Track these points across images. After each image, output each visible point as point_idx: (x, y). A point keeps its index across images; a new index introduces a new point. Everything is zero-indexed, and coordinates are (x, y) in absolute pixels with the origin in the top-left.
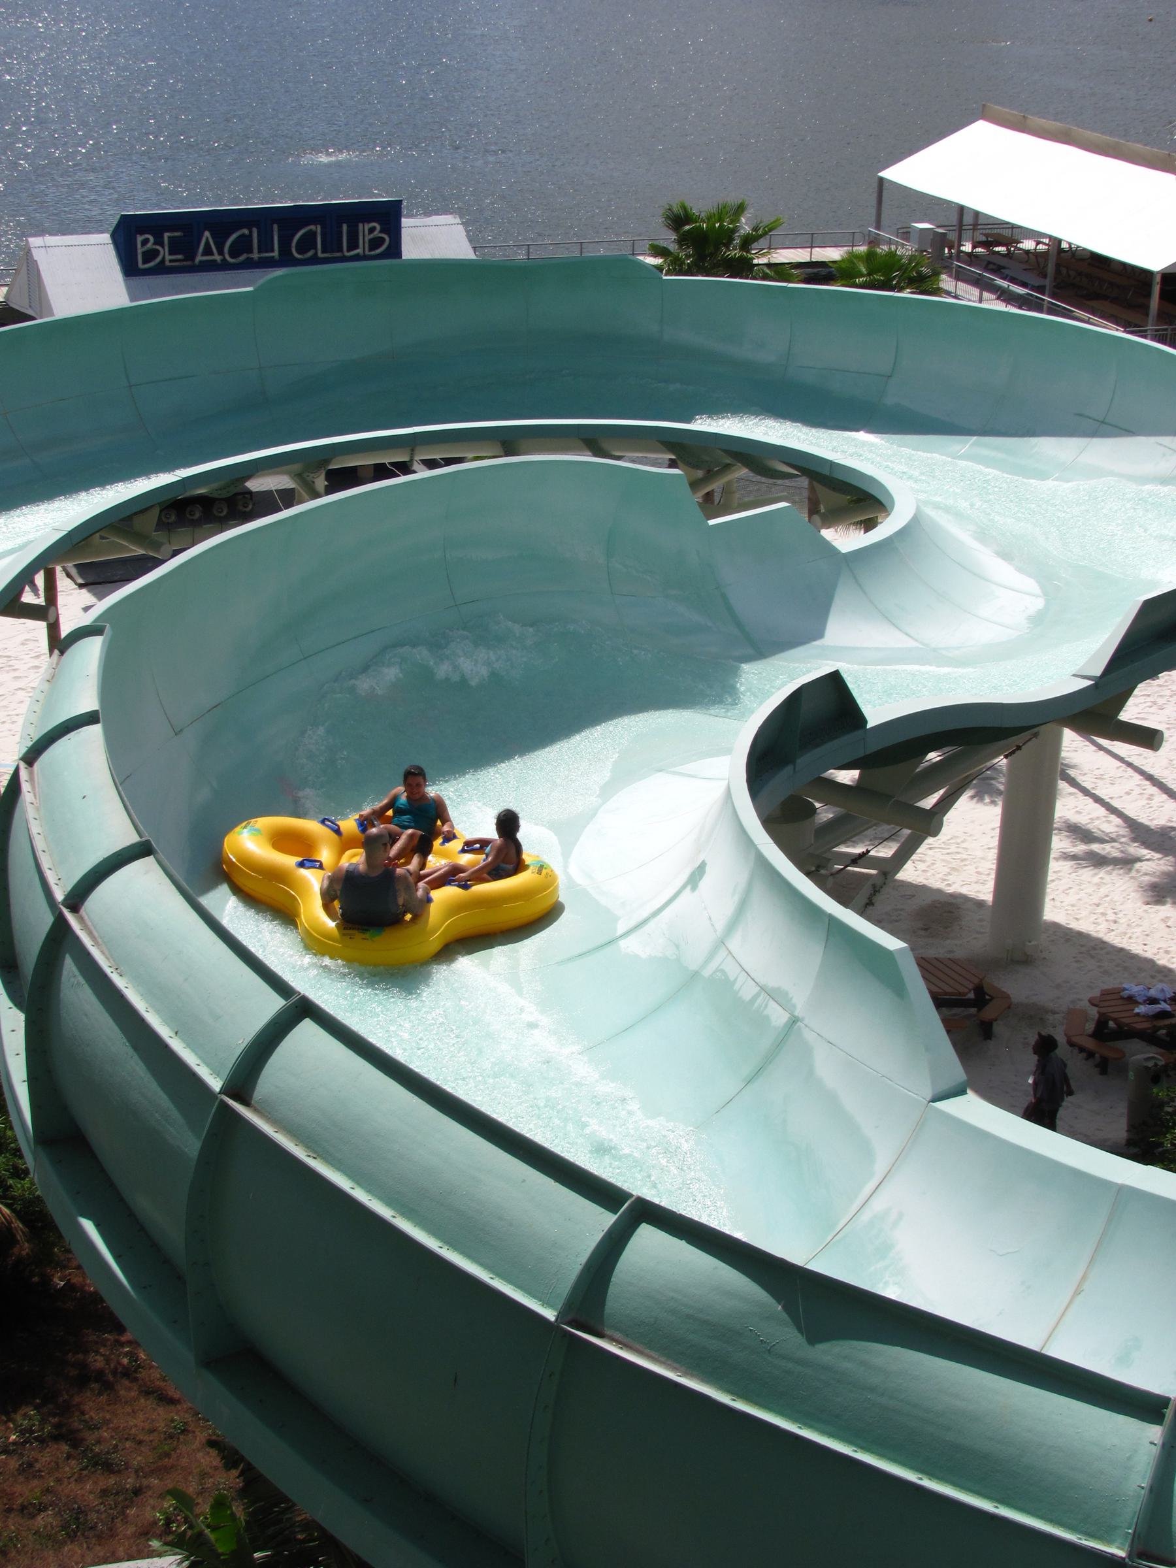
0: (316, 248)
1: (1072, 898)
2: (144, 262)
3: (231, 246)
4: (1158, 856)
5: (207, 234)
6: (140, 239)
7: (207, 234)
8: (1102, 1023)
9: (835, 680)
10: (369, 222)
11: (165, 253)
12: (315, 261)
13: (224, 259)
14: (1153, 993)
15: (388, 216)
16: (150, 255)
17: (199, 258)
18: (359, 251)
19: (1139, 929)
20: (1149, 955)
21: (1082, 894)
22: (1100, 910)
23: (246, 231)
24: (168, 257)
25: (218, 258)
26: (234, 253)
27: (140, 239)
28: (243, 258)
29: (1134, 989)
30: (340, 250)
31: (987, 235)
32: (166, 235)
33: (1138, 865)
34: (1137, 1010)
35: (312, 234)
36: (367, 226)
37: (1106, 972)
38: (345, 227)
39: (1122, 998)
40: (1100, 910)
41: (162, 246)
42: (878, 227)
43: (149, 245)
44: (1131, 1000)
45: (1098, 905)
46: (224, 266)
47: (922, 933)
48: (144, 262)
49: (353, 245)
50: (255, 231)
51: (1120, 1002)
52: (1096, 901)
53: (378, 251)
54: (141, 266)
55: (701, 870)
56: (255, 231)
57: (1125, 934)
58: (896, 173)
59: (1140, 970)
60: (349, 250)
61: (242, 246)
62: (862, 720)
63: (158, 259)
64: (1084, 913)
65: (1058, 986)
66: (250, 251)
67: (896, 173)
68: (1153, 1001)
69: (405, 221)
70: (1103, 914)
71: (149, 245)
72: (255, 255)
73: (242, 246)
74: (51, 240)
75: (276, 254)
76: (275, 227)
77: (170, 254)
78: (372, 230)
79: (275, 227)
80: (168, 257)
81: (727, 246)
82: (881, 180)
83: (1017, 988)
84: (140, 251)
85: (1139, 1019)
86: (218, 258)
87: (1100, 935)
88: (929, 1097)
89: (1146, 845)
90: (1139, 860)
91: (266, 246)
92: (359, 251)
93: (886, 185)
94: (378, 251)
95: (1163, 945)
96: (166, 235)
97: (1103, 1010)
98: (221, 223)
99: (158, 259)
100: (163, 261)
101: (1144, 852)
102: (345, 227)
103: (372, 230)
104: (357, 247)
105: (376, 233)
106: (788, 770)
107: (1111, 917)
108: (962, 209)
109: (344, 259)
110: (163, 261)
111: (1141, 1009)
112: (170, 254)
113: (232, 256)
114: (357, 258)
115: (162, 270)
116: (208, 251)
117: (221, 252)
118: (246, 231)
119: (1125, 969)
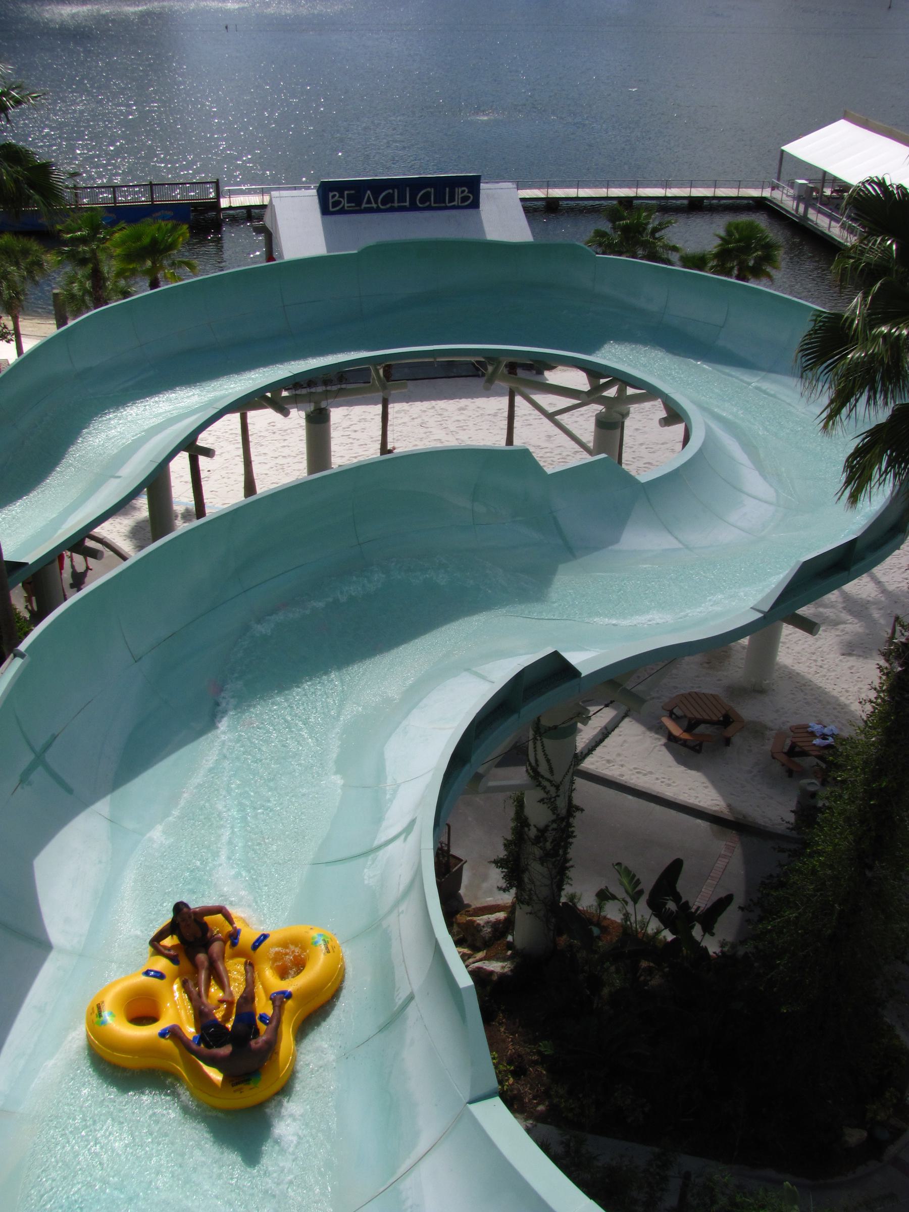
0: (430, 201)
1: (798, 648)
2: (333, 207)
3: (384, 197)
4: (856, 621)
5: (369, 192)
6: (331, 194)
7: (369, 192)
8: (793, 746)
9: (556, 655)
10: (461, 187)
11: (345, 203)
12: (430, 208)
13: (378, 207)
14: (826, 731)
15: (472, 184)
16: (336, 204)
17: (364, 205)
18: (455, 203)
19: (833, 674)
20: (835, 693)
21: (806, 646)
22: (814, 657)
23: (391, 191)
24: (346, 205)
25: (374, 205)
26: (383, 203)
27: (331, 194)
28: (388, 206)
29: (816, 728)
30: (444, 202)
31: (840, 186)
32: (346, 192)
33: (841, 627)
34: (814, 742)
35: (428, 194)
36: (460, 190)
37: (807, 703)
38: (447, 189)
39: (807, 732)
40: (814, 657)
41: (343, 197)
42: (778, 179)
43: (336, 198)
44: (813, 734)
45: (814, 654)
46: (378, 210)
47: (706, 665)
48: (333, 207)
49: (452, 199)
50: (396, 191)
51: (806, 735)
52: (813, 651)
53: (466, 204)
54: (331, 209)
55: (413, 822)
56: (396, 191)
57: (825, 676)
58: (792, 148)
59: (828, 703)
60: (450, 202)
61: (388, 199)
62: (580, 674)
63: (341, 206)
64: (804, 659)
65: (777, 711)
66: (393, 202)
67: (792, 148)
68: (824, 737)
69: (482, 186)
70: (815, 661)
71: (336, 198)
72: (396, 205)
73: (388, 199)
74: (284, 193)
75: (407, 204)
76: (408, 189)
77: (348, 202)
78: (463, 192)
79: (408, 189)
80: (346, 205)
81: (641, 233)
82: (783, 151)
83: (748, 711)
84: (331, 201)
85: (813, 748)
86: (374, 205)
87: (809, 676)
88: (468, 1099)
89: (851, 612)
90: (844, 623)
91: (402, 199)
92: (455, 203)
93: (784, 156)
94: (466, 204)
95: (846, 686)
96: (346, 192)
97: (794, 740)
98: (377, 186)
99: (341, 206)
100: (344, 206)
101: (850, 618)
102: (447, 189)
103: (463, 192)
104: (454, 201)
105: (466, 193)
106: (515, 716)
107: (819, 663)
108: (825, 173)
109: (446, 208)
110: (344, 206)
111: (817, 741)
112: (348, 202)
113: (382, 205)
114: (454, 207)
115: (342, 212)
116: (369, 202)
117: (376, 202)
118: (391, 191)
119: (820, 701)
